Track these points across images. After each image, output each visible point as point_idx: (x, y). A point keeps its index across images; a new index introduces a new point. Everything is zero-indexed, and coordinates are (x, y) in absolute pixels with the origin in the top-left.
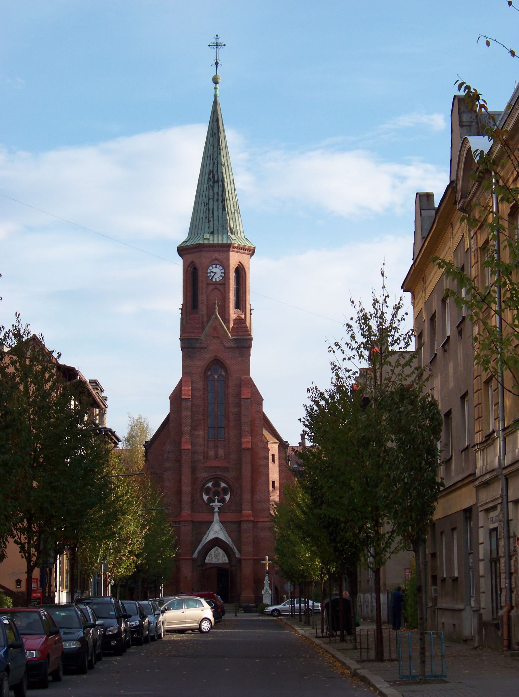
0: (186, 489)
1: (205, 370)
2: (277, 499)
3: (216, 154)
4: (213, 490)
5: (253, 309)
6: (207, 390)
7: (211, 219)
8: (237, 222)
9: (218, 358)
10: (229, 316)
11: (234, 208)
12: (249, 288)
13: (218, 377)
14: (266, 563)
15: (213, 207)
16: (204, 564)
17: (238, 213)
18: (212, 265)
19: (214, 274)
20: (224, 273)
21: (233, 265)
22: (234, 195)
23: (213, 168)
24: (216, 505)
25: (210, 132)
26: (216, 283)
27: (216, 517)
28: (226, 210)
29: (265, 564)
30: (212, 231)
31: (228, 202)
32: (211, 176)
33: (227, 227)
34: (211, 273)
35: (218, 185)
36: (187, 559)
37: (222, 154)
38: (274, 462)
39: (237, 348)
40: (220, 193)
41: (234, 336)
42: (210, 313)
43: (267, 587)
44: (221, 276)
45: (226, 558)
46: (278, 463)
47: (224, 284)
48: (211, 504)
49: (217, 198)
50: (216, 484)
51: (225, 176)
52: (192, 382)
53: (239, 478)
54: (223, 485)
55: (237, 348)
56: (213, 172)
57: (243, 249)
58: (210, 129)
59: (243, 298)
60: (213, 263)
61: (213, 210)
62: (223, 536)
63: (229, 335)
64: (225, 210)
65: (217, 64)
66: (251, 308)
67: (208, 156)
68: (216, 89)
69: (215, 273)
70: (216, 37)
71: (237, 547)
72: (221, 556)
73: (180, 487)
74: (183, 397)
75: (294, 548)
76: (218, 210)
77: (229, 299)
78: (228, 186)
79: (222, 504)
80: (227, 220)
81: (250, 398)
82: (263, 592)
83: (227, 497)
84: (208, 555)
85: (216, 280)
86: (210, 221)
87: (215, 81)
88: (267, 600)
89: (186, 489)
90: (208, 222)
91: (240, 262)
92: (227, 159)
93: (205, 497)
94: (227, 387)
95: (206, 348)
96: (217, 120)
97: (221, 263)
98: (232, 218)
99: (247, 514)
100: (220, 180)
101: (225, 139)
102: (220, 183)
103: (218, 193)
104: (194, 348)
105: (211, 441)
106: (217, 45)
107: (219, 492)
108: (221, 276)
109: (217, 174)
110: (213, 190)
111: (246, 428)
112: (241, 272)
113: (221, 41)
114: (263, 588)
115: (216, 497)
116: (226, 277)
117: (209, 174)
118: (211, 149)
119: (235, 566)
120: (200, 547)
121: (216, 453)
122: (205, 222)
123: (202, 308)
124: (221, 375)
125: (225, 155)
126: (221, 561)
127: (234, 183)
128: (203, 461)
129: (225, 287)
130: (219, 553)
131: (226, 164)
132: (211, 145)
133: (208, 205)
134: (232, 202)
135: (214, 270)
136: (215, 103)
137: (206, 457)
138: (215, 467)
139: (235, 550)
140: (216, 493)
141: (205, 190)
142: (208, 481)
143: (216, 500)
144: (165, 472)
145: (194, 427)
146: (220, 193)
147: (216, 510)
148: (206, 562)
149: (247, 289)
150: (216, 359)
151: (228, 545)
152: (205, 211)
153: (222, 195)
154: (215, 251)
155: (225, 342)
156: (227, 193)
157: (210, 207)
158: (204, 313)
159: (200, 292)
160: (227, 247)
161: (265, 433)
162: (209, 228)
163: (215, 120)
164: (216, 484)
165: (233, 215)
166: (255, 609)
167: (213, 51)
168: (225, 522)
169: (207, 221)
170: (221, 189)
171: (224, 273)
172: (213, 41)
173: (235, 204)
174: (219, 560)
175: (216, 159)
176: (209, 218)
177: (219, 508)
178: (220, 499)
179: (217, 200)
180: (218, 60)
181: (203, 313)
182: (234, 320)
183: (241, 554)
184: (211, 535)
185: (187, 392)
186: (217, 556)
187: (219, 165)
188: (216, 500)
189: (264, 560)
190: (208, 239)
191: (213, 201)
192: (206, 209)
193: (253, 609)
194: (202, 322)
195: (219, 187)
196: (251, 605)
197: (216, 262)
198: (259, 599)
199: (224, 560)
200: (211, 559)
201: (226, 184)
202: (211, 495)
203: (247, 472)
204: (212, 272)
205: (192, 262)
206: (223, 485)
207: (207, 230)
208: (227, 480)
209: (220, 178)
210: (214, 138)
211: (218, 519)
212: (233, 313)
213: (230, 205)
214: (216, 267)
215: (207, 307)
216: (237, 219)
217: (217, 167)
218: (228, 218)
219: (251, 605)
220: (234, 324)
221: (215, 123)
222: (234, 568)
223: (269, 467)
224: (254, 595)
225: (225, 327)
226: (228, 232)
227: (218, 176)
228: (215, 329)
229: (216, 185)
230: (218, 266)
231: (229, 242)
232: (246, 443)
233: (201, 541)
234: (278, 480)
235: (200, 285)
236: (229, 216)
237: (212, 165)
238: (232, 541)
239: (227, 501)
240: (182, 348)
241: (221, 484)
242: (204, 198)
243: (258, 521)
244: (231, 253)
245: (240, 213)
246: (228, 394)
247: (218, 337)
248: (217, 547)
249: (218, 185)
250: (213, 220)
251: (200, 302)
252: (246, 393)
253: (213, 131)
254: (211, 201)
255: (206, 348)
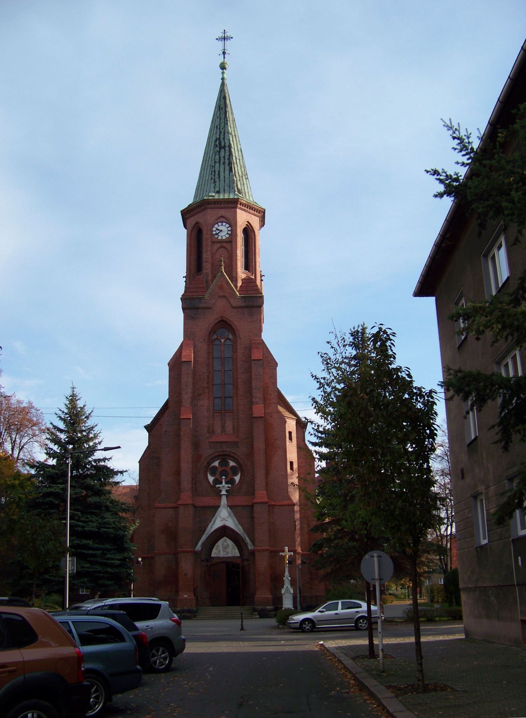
0: (186, 466)
1: (210, 333)
2: (296, 481)
3: (222, 125)
4: (220, 469)
5: (264, 276)
6: (213, 355)
7: (217, 180)
8: (245, 185)
9: (224, 319)
10: (237, 274)
11: (242, 173)
12: (259, 250)
13: (225, 341)
14: (286, 555)
15: (220, 169)
16: (209, 558)
17: (246, 178)
18: (218, 223)
19: (219, 231)
20: (231, 230)
21: (241, 225)
22: (241, 161)
23: (220, 135)
24: (224, 487)
25: (217, 108)
26: (222, 241)
27: (224, 501)
28: (233, 171)
29: (284, 557)
30: (218, 190)
31: (236, 165)
32: (218, 143)
33: (235, 187)
34: (217, 231)
35: (225, 150)
36: (188, 552)
37: (229, 124)
38: (292, 441)
39: (246, 307)
40: (227, 157)
41: (242, 294)
42: (216, 269)
43: (287, 584)
44: (227, 234)
45: (237, 551)
46: (296, 442)
47: (231, 242)
48: (218, 486)
49: (223, 161)
50: (224, 463)
51: (232, 143)
52: (195, 347)
53: (250, 454)
54: (232, 463)
55: (246, 307)
56: (219, 139)
57: (251, 208)
58: (217, 106)
59: (252, 260)
60: (218, 221)
61: (219, 172)
62: (232, 523)
63: (237, 293)
64: (232, 171)
65: (224, 53)
66: (262, 274)
67: (214, 127)
68: (223, 73)
69: (221, 231)
70: (223, 32)
71: (249, 537)
72: (230, 548)
73: (179, 467)
74: (182, 360)
75: (321, 530)
76: (224, 172)
77: (236, 256)
78: (235, 153)
79: (230, 485)
80: (234, 180)
81: (261, 360)
82: (283, 592)
83: (237, 478)
84: (215, 548)
85: (222, 238)
86: (216, 182)
87: (223, 67)
88: (288, 603)
89: (186, 466)
90: (214, 183)
91: (248, 222)
92: (234, 131)
93: (211, 479)
94: (235, 351)
95: (210, 308)
96: (225, 98)
97: (227, 219)
98: (240, 181)
99: (261, 495)
100: (227, 146)
101: (232, 113)
102: (227, 149)
103: (224, 157)
104: (198, 308)
105: (216, 412)
106: (224, 38)
107: (227, 472)
108: (227, 234)
109: (224, 141)
110: (219, 155)
111: (258, 395)
112: (249, 232)
113: (228, 34)
114: (283, 587)
115: (224, 477)
116: (231, 240)
117: (216, 141)
118: (217, 120)
119: (247, 560)
120: (204, 537)
121: (223, 427)
122: (211, 183)
123: (207, 267)
124: (228, 339)
125: (232, 127)
126: (230, 555)
127: (241, 152)
128: (208, 435)
129: (231, 245)
130: (228, 545)
131: (233, 134)
132: (218, 118)
133: (213, 168)
134: (239, 166)
135: (220, 228)
136: (223, 84)
137: (212, 432)
138: (221, 442)
139: (248, 540)
140: (224, 473)
141: (211, 156)
142: (213, 460)
143: (224, 481)
144: (162, 449)
145: (195, 397)
146: (227, 157)
147: (224, 492)
148: (212, 555)
149: (257, 251)
150: (222, 321)
151: (237, 534)
152: (210, 173)
153: (229, 159)
154: (219, 208)
155: (232, 301)
156: (234, 158)
157: (216, 170)
158: (209, 271)
159: (204, 250)
160: (234, 203)
161: (281, 409)
162: (214, 188)
163: (222, 97)
164: (224, 463)
165: (241, 178)
166: (273, 613)
167: (221, 43)
168: (235, 506)
169: (213, 182)
170: (227, 153)
171: (231, 230)
172: (221, 35)
173: (243, 169)
174: (228, 553)
175: (223, 128)
176: (214, 179)
177: (227, 491)
178: (228, 480)
179: (224, 163)
180: (225, 51)
181: (207, 271)
182: (242, 280)
183: (254, 545)
184: (217, 523)
185: (189, 355)
186: (225, 548)
187: (226, 134)
188: (224, 481)
189: (284, 551)
190: (213, 196)
191: (220, 164)
192: (212, 171)
193: (271, 613)
194: (207, 282)
195: (226, 152)
196: (268, 607)
197: (222, 220)
198: (278, 600)
199: (234, 553)
200: (219, 552)
201: (233, 150)
202: (218, 476)
203: (259, 444)
204: (218, 230)
205: (197, 223)
206: (232, 463)
207: (213, 190)
208: (236, 456)
209: (227, 144)
210: (221, 111)
211: (226, 503)
212: (241, 273)
213: (237, 169)
214: (222, 225)
215: (213, 265)
216: (245, 182)
217: (224, 135)
218: (235, 179)
219: (268, 607)
220: (242, 283)
221: (222, 100)
222: (246, 563)
223: (286, 446)
224: (272, 594)
225: (232, 286)
226: (235, 191)
227: (225, 143)
228: (221, 287)
229: (223, 151)
230: (224, 224)
231: (236, 197)
232: (258, 410)
233: (205, 530)
234: (297, 461)
235: (204, 243)
236: (236, 177)
237: (218, 134)
238: (244, 529)
239: (237, 483)
240: (184, 309)
241: (229, 462)
242: (210, 162)
243: (274, 505)
244: (239, 211)
245: (248, 179)
246: (236, 359)
247: (224, 297)
248: (225, 538)
249: (225, 150)
250: (219, 181)
251: (204, 260)
252: (256, 355)
253: (220, 106)
254: (217, 165)
255: (210, 308)
